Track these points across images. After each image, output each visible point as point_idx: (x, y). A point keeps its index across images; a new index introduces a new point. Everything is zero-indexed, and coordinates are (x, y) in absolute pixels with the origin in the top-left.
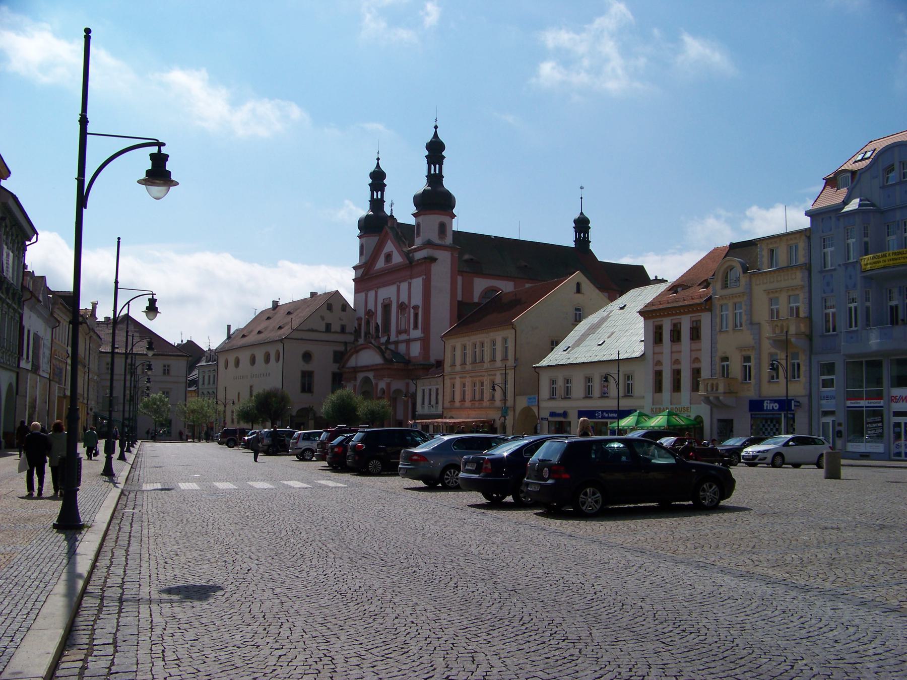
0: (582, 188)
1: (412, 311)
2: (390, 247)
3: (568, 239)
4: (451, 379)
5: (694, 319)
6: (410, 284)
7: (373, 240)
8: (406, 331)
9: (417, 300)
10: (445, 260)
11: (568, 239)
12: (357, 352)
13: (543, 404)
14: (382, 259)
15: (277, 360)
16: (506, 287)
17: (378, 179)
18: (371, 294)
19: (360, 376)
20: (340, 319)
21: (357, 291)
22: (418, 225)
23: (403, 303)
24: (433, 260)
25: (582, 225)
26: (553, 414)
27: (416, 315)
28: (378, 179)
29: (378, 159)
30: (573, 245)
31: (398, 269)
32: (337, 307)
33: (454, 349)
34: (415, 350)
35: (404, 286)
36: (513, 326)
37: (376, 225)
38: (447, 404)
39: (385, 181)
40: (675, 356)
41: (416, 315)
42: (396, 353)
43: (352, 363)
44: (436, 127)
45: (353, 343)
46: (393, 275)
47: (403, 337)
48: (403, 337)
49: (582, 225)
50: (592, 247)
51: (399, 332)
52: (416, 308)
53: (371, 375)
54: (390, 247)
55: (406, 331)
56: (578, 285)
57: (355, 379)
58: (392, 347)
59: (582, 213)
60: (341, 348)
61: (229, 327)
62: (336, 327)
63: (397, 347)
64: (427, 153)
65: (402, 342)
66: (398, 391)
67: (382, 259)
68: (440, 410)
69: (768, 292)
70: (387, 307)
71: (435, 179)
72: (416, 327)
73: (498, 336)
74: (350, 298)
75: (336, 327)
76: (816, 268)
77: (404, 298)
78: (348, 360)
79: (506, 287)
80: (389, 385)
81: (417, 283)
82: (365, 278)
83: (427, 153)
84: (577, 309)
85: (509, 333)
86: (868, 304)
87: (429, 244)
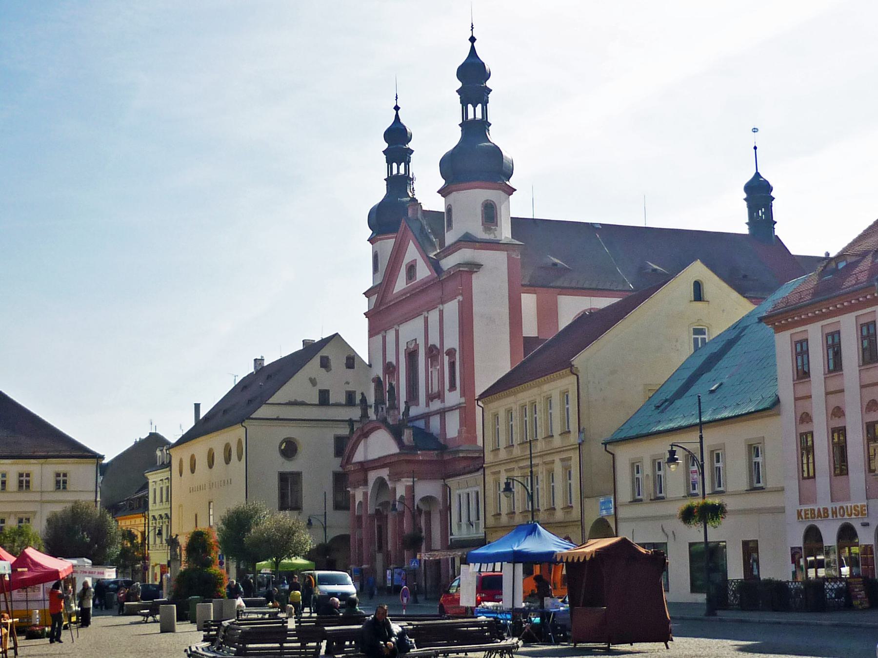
1: (446, 358)
2: (412, 253)
3: (734, 219)
4: (494, 473)
5: (864, 320)
7: (388, 244)
8: (440, 396)
9: (452, 341)
10: (495, 263)
11: (734, 219)
15: (240, 459)
17: (397, 141)
18: (391, 335)
19: (373, 476)
21: (373, 332)
22: (449, 210)
24: (474, 267)
25: (759, 193)
27: (452, 365)
28: (397, 141)
29: (397, 108)
30: (745, 230)
31: (425, 287)
32: (337, 362)
34: (453, 428)
35: (434, 316)
37: (392, 216)
38: (491, 521)
40: (834, 401)
41: (452, 365)
43: (359, 456)
44: (473, 39)
46: (424, 297)
47: (436, 405)
48: (436, 405)
49: (759, 193)
50: (779, 231)
51: (430, 398)
52: (451, 353)
53: (384, 473)
54: (412, 253)
57: (365, 482)
58: (421, 424)
59: (757, 175)
60: (344, 431)
61: (197, 407)
62: (337, 396)
63: (427, 424)
66: (428, 500)
68: (481, 534)
70: (412, 356)
71: (475, 130)
72: (452, 387)
74: (359, 342)
75: (337, 396)
77: (434, 340)
80: (411, 490)
81: (451, 308)
82: (383, 311)
85: (567, 382)
87: (468, 240)
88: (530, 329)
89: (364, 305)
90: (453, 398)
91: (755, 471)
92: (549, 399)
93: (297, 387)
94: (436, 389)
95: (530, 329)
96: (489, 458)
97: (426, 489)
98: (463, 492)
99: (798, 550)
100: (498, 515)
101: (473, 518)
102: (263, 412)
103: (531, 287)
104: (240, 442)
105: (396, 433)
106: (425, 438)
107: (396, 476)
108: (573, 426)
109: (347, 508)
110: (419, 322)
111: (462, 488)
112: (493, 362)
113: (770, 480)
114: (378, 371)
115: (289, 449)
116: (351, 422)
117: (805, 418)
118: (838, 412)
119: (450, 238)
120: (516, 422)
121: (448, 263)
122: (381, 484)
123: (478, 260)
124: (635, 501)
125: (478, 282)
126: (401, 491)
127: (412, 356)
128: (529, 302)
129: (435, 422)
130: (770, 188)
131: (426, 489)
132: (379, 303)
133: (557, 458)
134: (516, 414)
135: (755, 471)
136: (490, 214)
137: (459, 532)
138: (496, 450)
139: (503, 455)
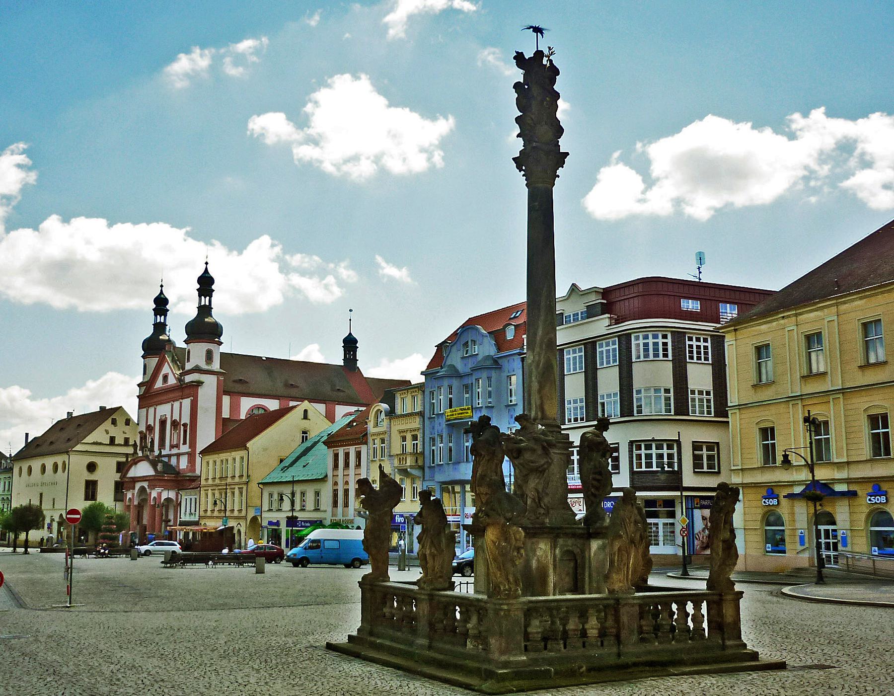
0: (351, 310)
1: (182, 428)
2: (166, 369)
3: (337, 359)
6: (181, 403)
7: (153, 361)
8: (177, 446)
9: (186, 419)
12: (136, 463)
13: (264, 515)
14: (161, 378)
15: (64, 472)
16: (273, 405)
17: (161, 304)
18: (151, 410)
19: (138, 486)
20: (124, 433)
23: (175, 421)
24: (200, 383)
25: (350, 344)
26: (270, 523)
27: (185, 432)
28: (161, 304)
29: (162, 286)
31: (172, 389)
33: (208, 463)
34: (184, 463)
35: (176, 405)
36: (247, 449)
37: (155, 346)
38: (202, 514)
39: (213, 287)
41: (185, 432)
42: (167, 466)
43: (132, 473)
45: (133, 454)
49: (350, 344)
52: (185, 425)
53: (145, 484)
55: (177, 446)
56: (306, 411)
57: (134, 489)
58: (166, 459)
59: (350, 334)
61: (27, 435)
62: (119, 440)
63: (169, 460)
64: (198, 286)
65: (174, 455)
66: (168, 500)
67: (161, 378)
69: (400, 432)
70: (163, 423)
71: (205, 310)
72: (185, 443)
73: (238, 454)
74: (132, 408)
75: (119, 440)
76: (427, 415)
77: (176, 417)
78: (128, 471)
79: (273, 405)
80: (160, 494)
81: (187, 402)
82: (148, 396)
83: (198, 286)
84: (304, 433)
85: (243, 453)
86: (451, 445)
87: (197, 370)
88: (226, 414)
89: (137, 391)
90: (185, 448)
91: (317, 502)
92: (234, 459)
93: (99, 435)
94: (175, 443)
95: (226, 414)
96: (203, 482)
97: (172, 495)
98: (188, 498)
99: (770, 535)
100: (206, 511)
101: (193, 511)
102: (79, 447)
103: (226, 393)
104: (64, 462)
105: (154, 464)
106: (168, 467)
107: (152, 487)
108: (245, 474)
109: (122, 501)
110: (169, 406)
111: (186, 498)
112: (207, 435)
113: (322, 508)
114: (143, 428)
115: (92, 467)
116: (127, 455)
117: (336, 484)
118: (347, 483)
119: (188, 366)
120: (218, 467)
121: (188, 379)
122: (143, 489)
123: (202, 380)
124: (270, 510)
125: (201, 391)
126: (154, 494)
127: (163, 423)
128: (226, 400)
129: (174, 461)
130: (356, 341)
131: (172, 495)
132: (146, 392)
133: (237, 487)
134: (218, 463)
135: (317, 502)
136: (209, 356)
137: (185, 518)
138: (207, 479)
139: (210, 482)
